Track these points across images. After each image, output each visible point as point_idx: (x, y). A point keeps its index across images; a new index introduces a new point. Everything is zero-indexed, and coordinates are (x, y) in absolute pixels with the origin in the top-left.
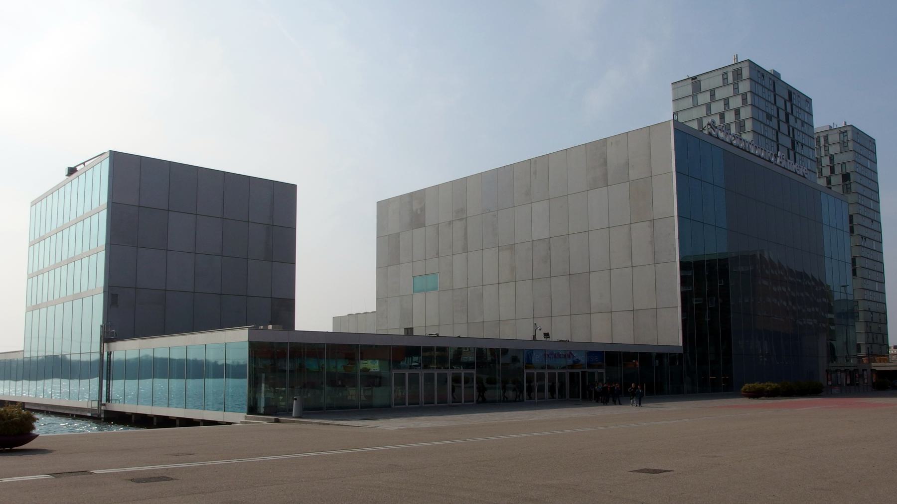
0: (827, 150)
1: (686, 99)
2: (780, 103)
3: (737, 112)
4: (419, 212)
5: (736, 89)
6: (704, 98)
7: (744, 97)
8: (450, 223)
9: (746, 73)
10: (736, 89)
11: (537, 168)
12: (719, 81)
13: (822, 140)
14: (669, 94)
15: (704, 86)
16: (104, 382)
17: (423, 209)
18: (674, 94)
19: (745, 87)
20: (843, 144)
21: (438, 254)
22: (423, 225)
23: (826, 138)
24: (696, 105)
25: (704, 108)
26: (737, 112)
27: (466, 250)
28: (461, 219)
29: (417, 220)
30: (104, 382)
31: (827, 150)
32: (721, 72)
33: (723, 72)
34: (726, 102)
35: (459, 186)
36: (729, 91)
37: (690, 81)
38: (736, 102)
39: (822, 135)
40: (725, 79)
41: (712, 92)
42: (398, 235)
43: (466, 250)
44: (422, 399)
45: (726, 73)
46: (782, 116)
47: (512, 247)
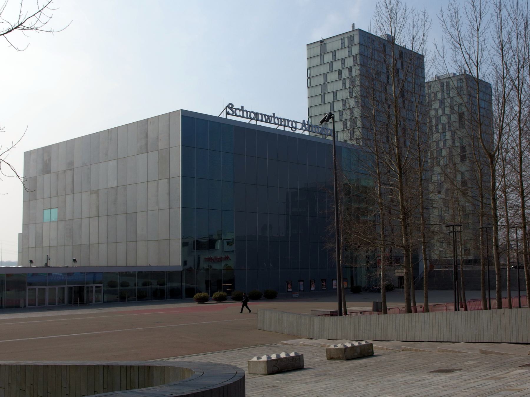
0: (448, 94)
1: (316, 58)
2: (391, 61)
3: (350, 70)
4: (48, 161)
5: (350, 51)
6: (328, 58)
7: (355, 57)
8: (65, 171)
9: (357, 39)
10: (350, 51)
11: (111, 135)
12: (337, 44)
13: (445, 84)
14: (304, 53)
15: (329, 48)
16: (487, 292)
17: (50, 160)
18: (309, 53)
19: (356, 50)
20: (459, 91)
21: (57, 194)
22: (49, 172)
23: (448, 83)
24: (323, 63)
25: (328, 66)
26: (350, 70)
27: (73, 192)
28: (71, 170)
29: (46, 169)
30: (487, 292)
31: (448, 94)
32: (340, 38)
33: (341, 37)
34: (343, 61)
35: (70, 144)
36: (343, 54)
37: (319, 44)
38: (350, 62)
39: (445, 81)
40: (343, 43)
41: (334, 53)
42: (35, 178)
43: (73, 192)
44: (47, 302)
45: (344, 39)
46: (391, 72)
47: (97, 192)
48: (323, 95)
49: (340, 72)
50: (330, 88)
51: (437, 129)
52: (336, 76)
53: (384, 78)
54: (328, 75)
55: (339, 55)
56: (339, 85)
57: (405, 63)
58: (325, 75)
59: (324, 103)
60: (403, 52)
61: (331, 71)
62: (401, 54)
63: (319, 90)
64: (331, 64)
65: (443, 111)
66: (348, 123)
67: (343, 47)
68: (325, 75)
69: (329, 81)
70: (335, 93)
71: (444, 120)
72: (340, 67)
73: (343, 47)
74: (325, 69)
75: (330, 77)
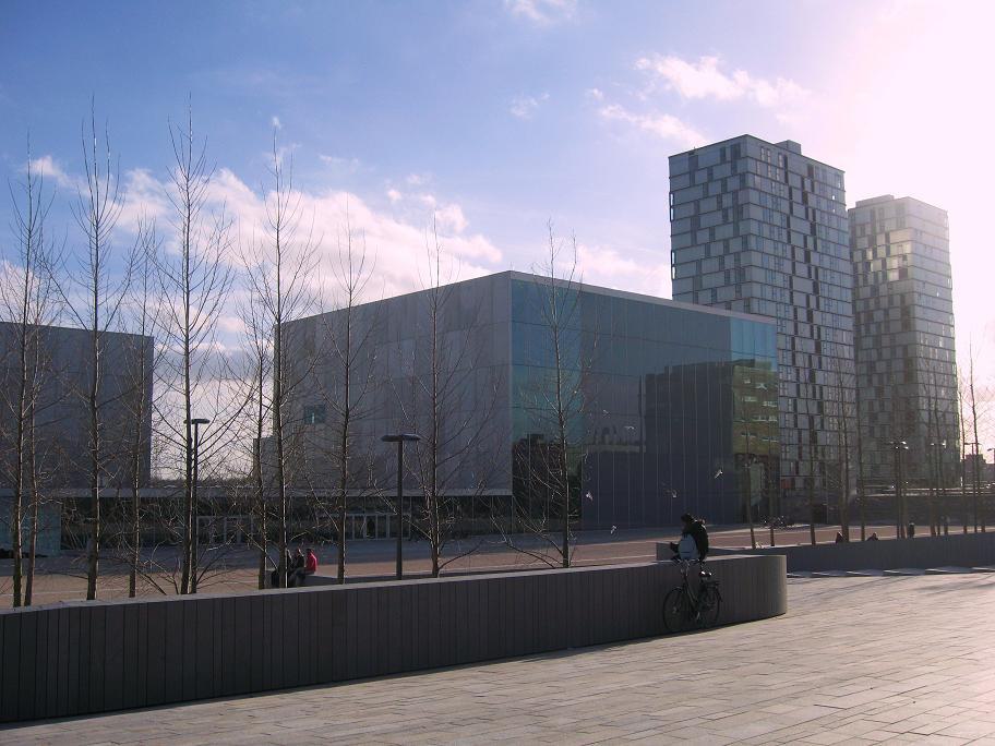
48: (691, 174)
49: (721, 258)
50: (705, 222)
51: (868, 330)
52: (712, 204)
53: (785, 207)
54: (702, 203)
55: (717, 174)
56: (719, 279)
57: (819, 242)
58: (697, 203)
59: (693, 184)
60: (812, 167)
61: (708, 256)
62: (810, 169)
63: (687, 226)
64: (706, 185)
65: (882, 405)
66: (732, 274)
67: (727, 284)
68: (697, 203)
69: (702, 211)
70: (712, 230)
71: (883, 418)
72: (719, 191)
73: (727, 284)
74: (697, 193)
75: (705, 206)
